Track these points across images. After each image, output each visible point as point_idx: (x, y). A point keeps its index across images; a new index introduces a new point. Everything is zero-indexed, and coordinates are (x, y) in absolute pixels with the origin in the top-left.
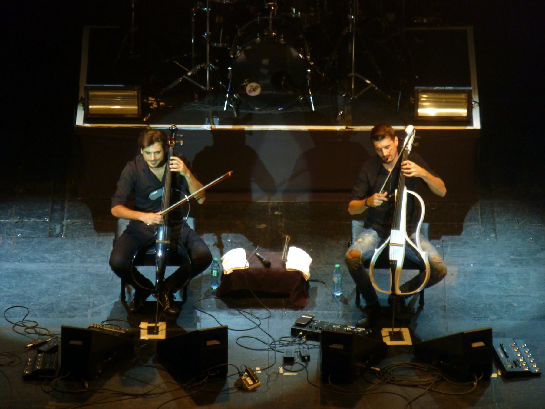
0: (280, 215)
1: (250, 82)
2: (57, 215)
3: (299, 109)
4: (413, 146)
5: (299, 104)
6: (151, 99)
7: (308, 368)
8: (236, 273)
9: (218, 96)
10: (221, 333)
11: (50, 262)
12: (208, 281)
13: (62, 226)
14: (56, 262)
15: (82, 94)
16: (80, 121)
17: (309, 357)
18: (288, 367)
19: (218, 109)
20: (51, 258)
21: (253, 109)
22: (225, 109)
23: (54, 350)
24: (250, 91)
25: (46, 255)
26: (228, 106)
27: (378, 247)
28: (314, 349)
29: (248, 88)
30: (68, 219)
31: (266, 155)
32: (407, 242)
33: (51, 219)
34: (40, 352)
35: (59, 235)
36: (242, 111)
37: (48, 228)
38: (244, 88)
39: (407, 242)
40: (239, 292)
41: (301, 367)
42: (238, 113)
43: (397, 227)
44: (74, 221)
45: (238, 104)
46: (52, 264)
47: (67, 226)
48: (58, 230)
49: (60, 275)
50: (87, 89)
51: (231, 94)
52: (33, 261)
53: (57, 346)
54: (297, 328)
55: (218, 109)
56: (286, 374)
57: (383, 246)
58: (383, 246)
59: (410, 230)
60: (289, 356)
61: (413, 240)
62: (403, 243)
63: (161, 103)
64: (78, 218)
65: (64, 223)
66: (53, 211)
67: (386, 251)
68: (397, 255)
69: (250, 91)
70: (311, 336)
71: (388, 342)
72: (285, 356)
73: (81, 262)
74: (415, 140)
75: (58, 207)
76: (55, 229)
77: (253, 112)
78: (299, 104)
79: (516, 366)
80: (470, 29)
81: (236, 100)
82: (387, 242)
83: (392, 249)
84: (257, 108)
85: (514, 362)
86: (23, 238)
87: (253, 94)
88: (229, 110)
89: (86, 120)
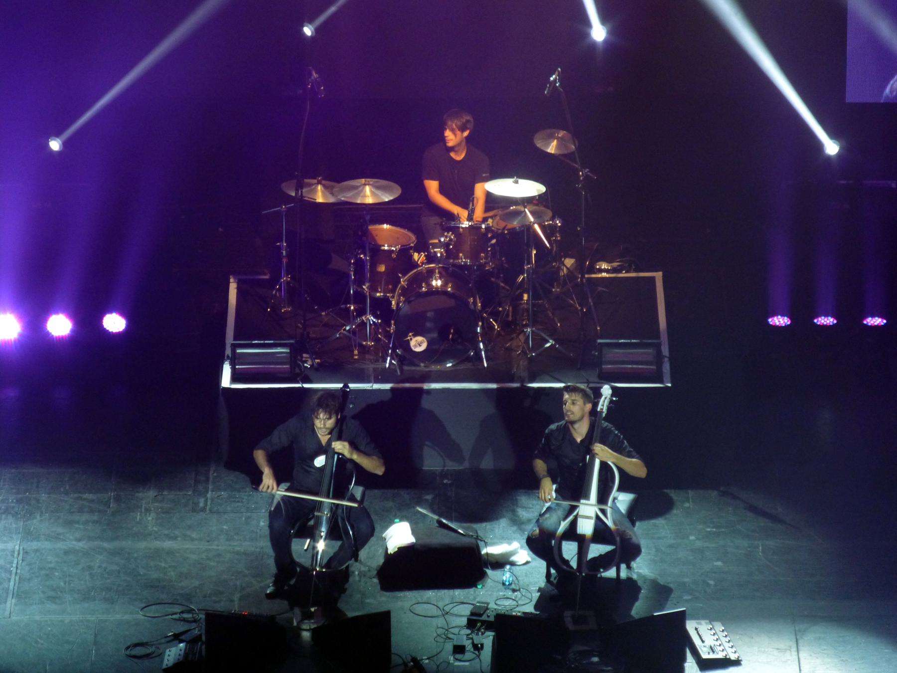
0: (450, 484)
1: (415, 336)
2: (201, 488)
3: (468, 365)
4: (609, 409)
5: (468, 359)
6: (304, 355)
7: (482, 657)
8: (403, 551)
9: (380, 352)
10: (383, 619)
11: (192, 540)
12: (370, 558)
13: (207, 499)
14: (200, 540)
15: (228, 352)
16: (226, 381)
17: (482, 645)
18: (459, 656)
19: (379, 365)
20: (194, 535)
21: (419, 366)
22: (387, 365)
23: (197, 639)
24: (415, 346)
25: (188, 533)
26: (391, 363)
27: (565, 519)
28: (488, 639)
29: (412, 343)
30: (213, 491)
31: (326, 505)
32: (597, 517)
33: (194, 491)
34: (181, 641)
35: (203, 510)
36: (406, 368)
37: (191, 502)
38: (408, 342)
39: (597, 517)
40: (405, 570)
41: (473, 656)
42: (402, 370)
43: (587, 497)
44: (219, 493)
45: (402, 360)
46: (196, 542)
47: (212, 500)
48: (201, 505)
49: (204, 556)
50: (234, 347)
51: (394, 350)
52: (175, 538)
53: (201, 635)
54: (474, 618)
55: (379, 365)
56: (457, 663)
57: (571, 518)
58: (571, 518)
59: (602, 498)
60: (459, 643)
61: (603, 512)
62: (594, 515)
63: (317, 361)
64: (225, 490)
65: (209, 495)
66: (197, 482)
67: (574, 524)
68: (586, 527)
69: (415, 346)
70: (489, 626)
71: (571, 627)
72: (455, 643)
73: (227, 540)
74: (611, 402)
75: (202, 478)
76: (198, 503)
77: (418, 368)
78: (468, 359)
79: (713, 652)
80: (658, 276)
81: (400, 356)
82: (575, 513)
83: (580, 521)
84: (422, 365)
85: (711, 647)
86: (163, 513)
87: (419, 349)
88: (392, 367)
89: (235, 378)
